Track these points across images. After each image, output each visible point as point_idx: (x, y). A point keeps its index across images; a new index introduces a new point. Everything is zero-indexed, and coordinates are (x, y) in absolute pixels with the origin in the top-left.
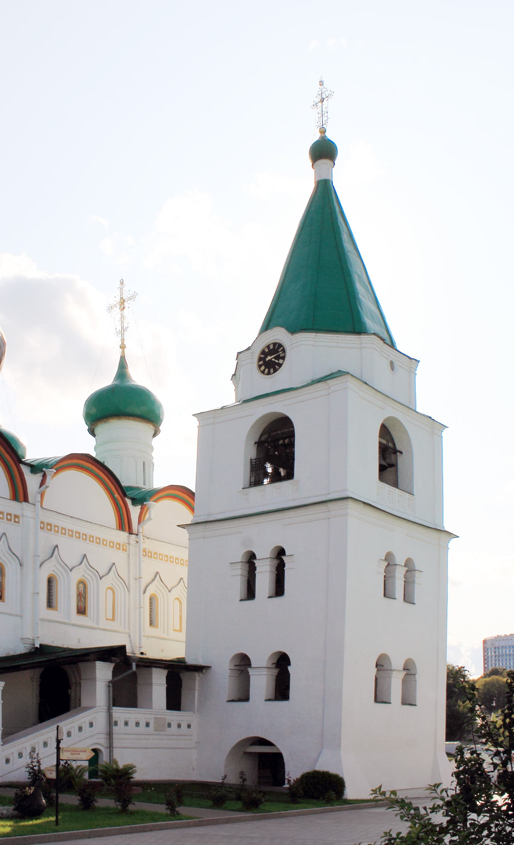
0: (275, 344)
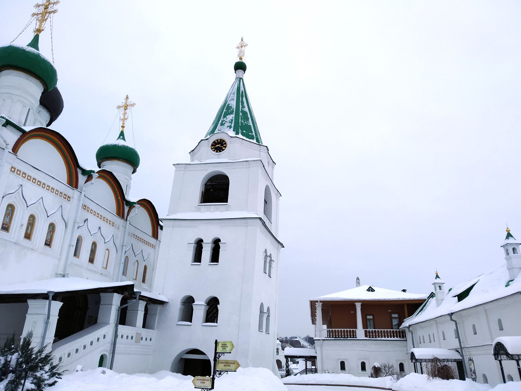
0: (221, 140)
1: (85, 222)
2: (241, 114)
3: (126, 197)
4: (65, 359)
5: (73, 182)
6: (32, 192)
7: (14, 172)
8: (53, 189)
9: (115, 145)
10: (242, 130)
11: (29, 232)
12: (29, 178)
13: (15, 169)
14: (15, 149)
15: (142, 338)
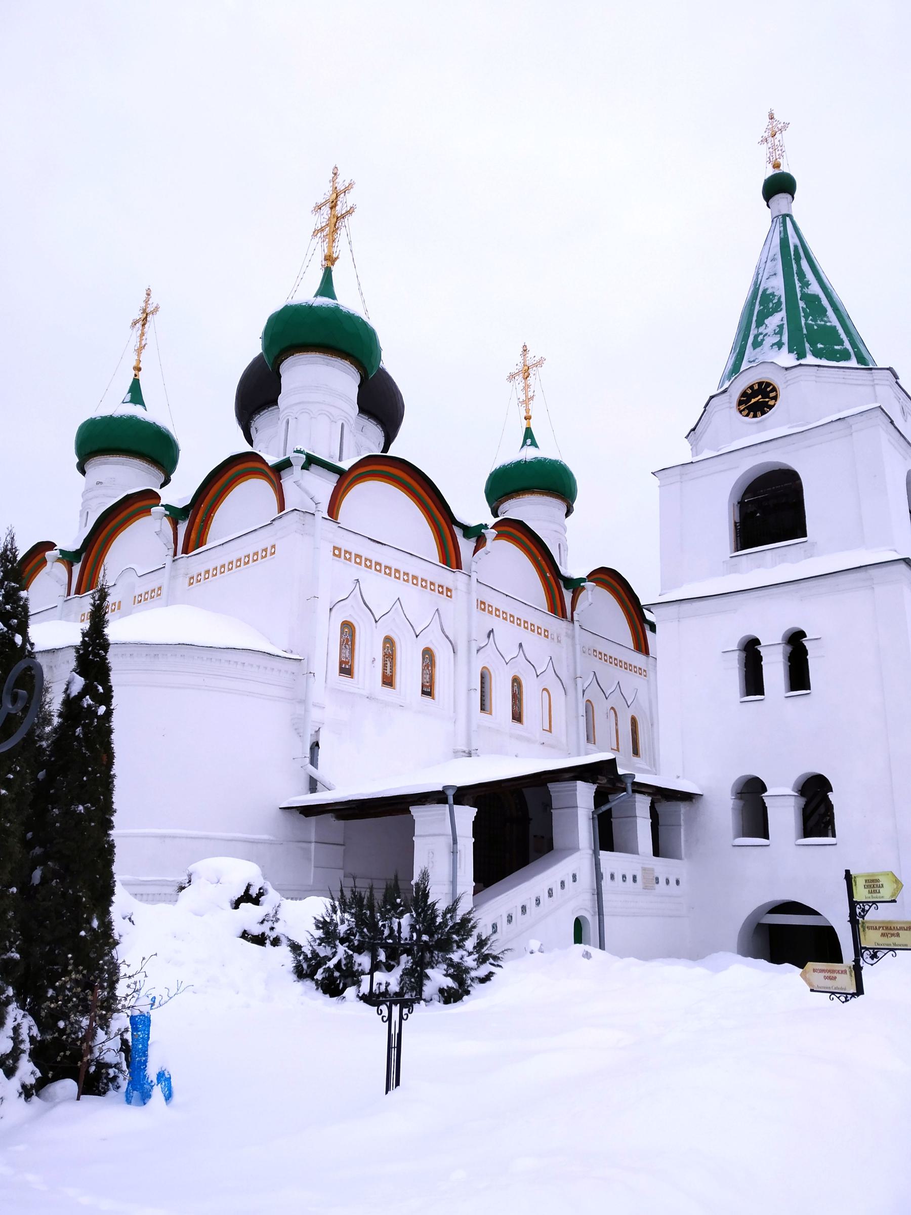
1: (489, 636)
2: (802, 304)
3: (564, 571)
4: (503, 925)
5: (450, 558)
6: (380, 591)
7: (339, 556)
8: (414, 577)
9: (518, 463)
11: (388, 671)
12: (369, 564)
13: (340, 550)
14: (333, 511)
15: (657, 879)
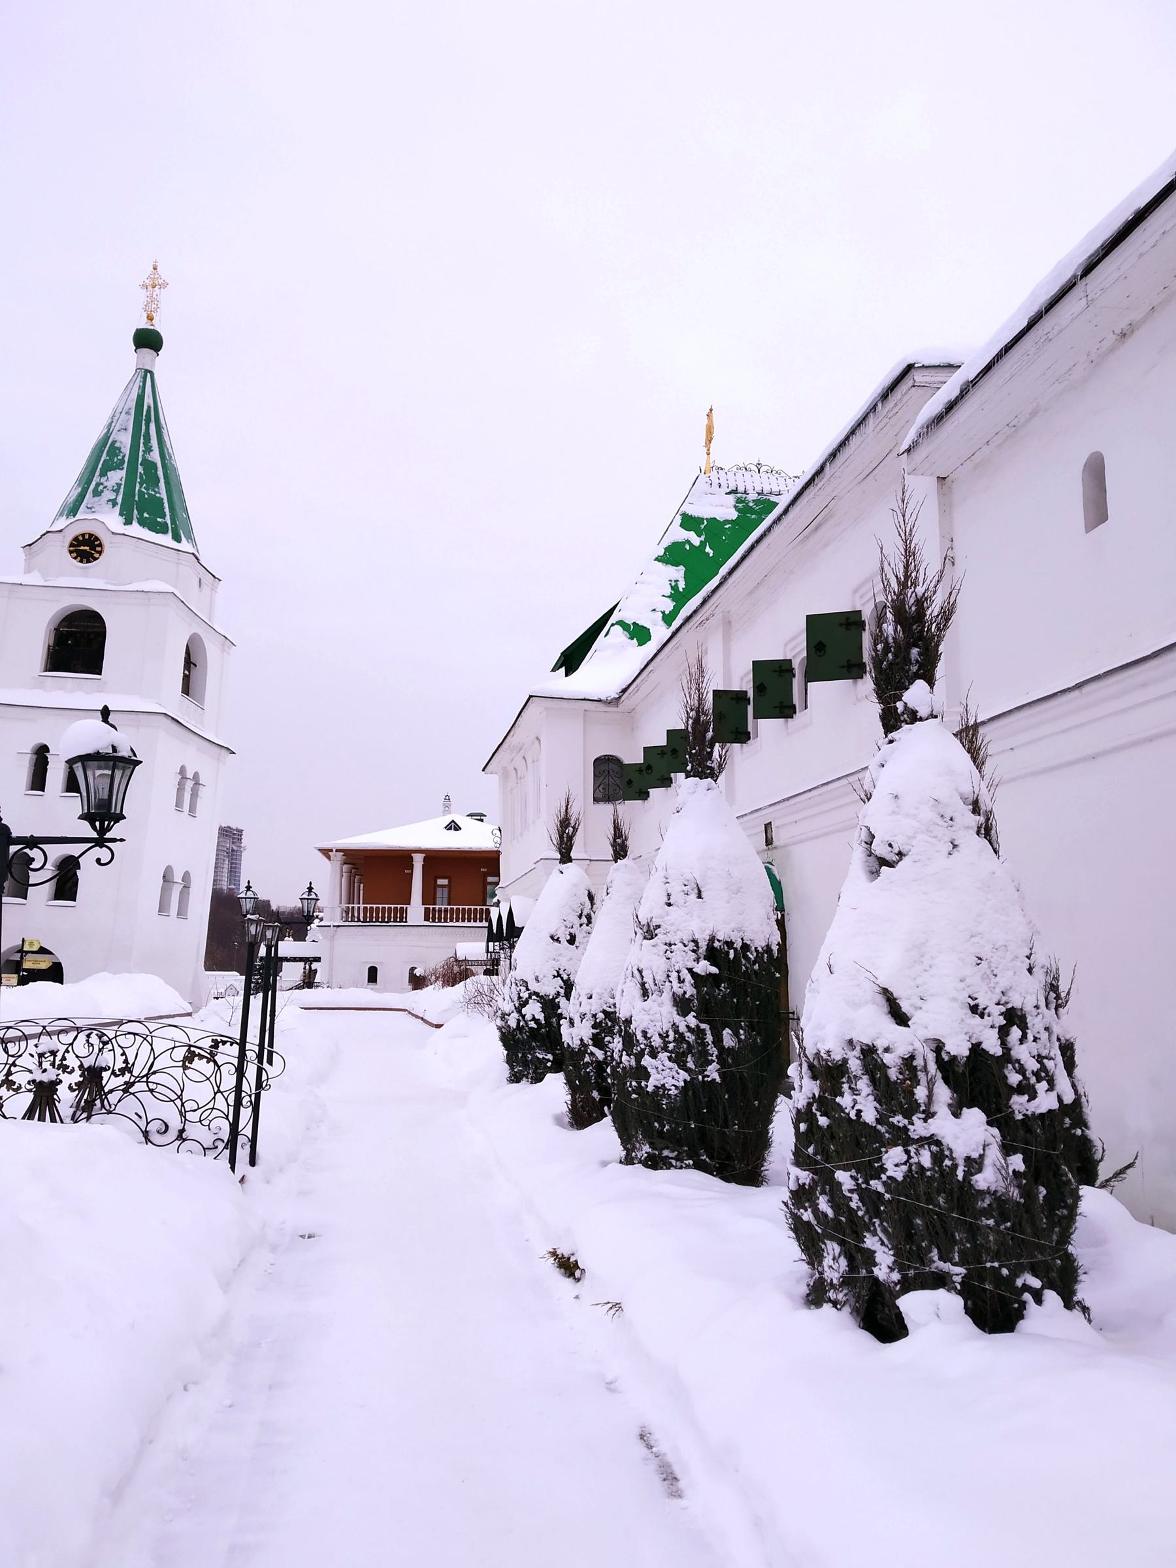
0: (91, 535)
2: (140, 469)
10: (140, 513)
